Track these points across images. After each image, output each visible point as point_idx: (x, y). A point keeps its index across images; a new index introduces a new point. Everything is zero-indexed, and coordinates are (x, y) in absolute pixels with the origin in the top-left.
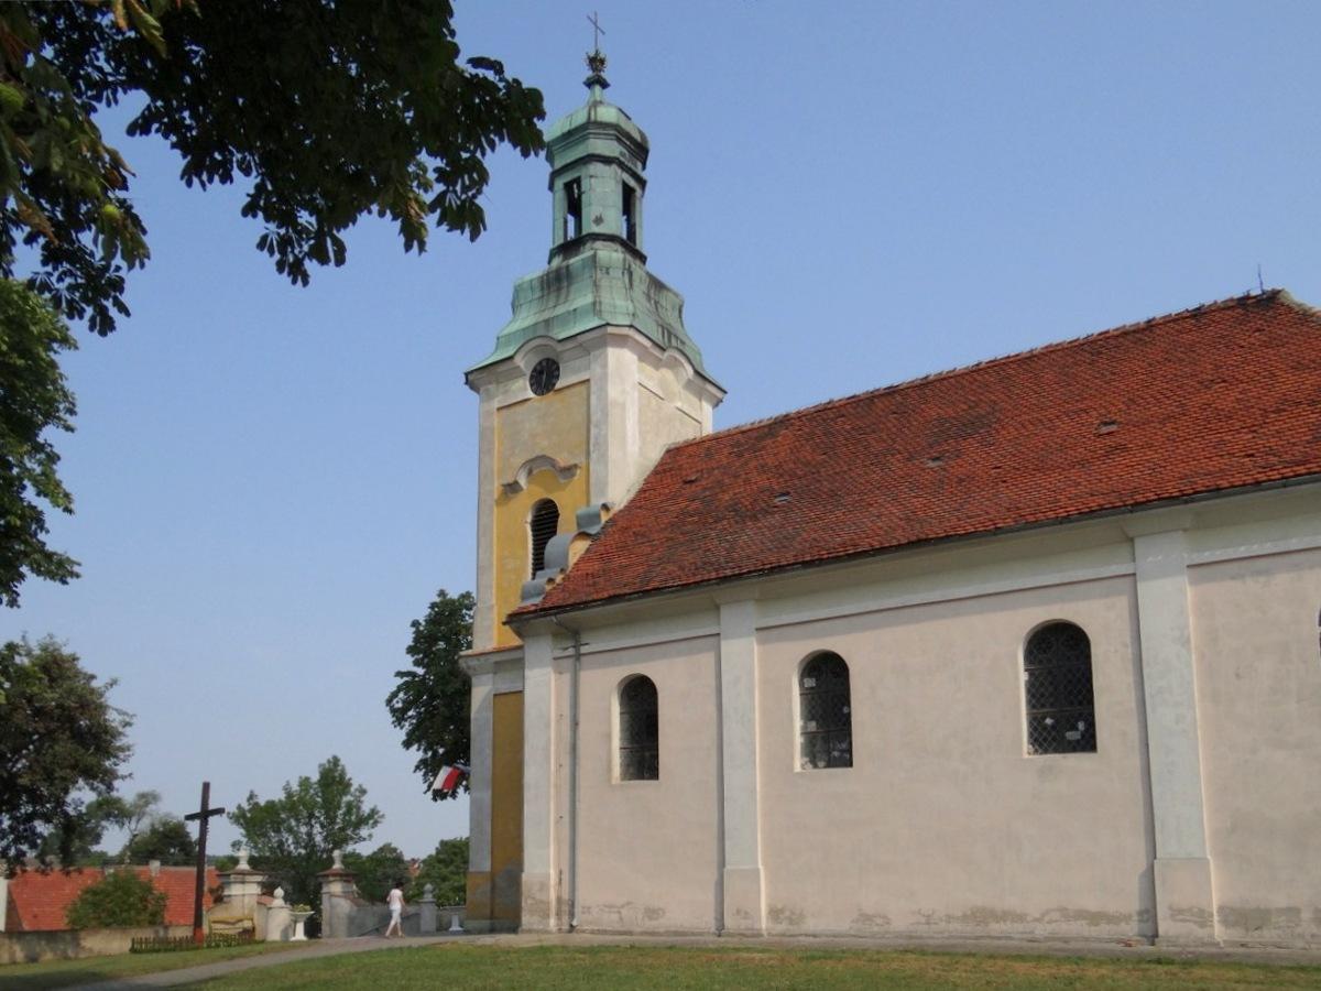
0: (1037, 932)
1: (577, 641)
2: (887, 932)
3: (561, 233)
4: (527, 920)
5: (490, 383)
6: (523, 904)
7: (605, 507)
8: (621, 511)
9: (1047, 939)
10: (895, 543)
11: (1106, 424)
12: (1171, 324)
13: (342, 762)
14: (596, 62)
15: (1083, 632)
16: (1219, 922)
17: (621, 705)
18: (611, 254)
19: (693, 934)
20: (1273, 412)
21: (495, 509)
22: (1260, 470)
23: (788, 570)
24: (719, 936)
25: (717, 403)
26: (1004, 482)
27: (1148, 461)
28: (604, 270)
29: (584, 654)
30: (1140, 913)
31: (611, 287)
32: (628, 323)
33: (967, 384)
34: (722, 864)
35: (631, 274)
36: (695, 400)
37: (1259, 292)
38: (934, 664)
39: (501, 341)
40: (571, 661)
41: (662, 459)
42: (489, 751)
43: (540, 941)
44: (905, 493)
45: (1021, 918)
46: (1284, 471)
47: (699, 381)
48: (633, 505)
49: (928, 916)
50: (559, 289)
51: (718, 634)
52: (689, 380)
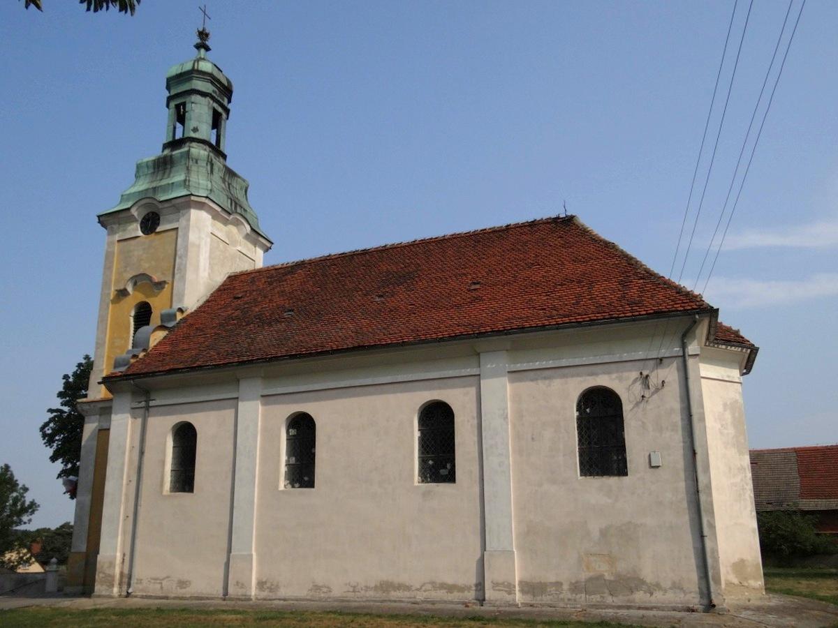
0: (418, 597)
1: (147, 401)
2: (329, 598)
3: (171, 134)
4: (99, 588)
5: (114, 223)
6: (97, 577)
7: (181, 310)
8: (192, 313)
9: (423, 602)
10: (345, 347)
11: (475, 284)
12: (518, 229)
13: (11, 469)
14: (203, 35)
15: (450, 407)
16: (519, 591)
17: (174, 441)
18: (199, 151)
19: (208, 598)
20: (559, 285)
21: (110, 305)
22: (547, 318)
23: (197, 370)
24: (224, 600)
25: (267, 250)
26: (415, 314)
27: (492, 308)
28: (194, 161)
29: (151, 407)
30: (476, 585)
31: (198, 172)
32: (205, 195)
33: (406, 252)
34: (229, 551)
35: (212, 165)
36: (250, 246)
37: (564, 216)
38: (370, 423)
39: (124, 198)
40: (143, 410)
41: (225, 281)
42: (92, 468)
43: (95, 605)
44: (359, 316)
45: (408, 588)
46: (559, 320)
47: (254, 235)
48: (201, 310)
49: (354, 587)
50: (165, 169)
51: (237, 398)
52: (248, 234)
